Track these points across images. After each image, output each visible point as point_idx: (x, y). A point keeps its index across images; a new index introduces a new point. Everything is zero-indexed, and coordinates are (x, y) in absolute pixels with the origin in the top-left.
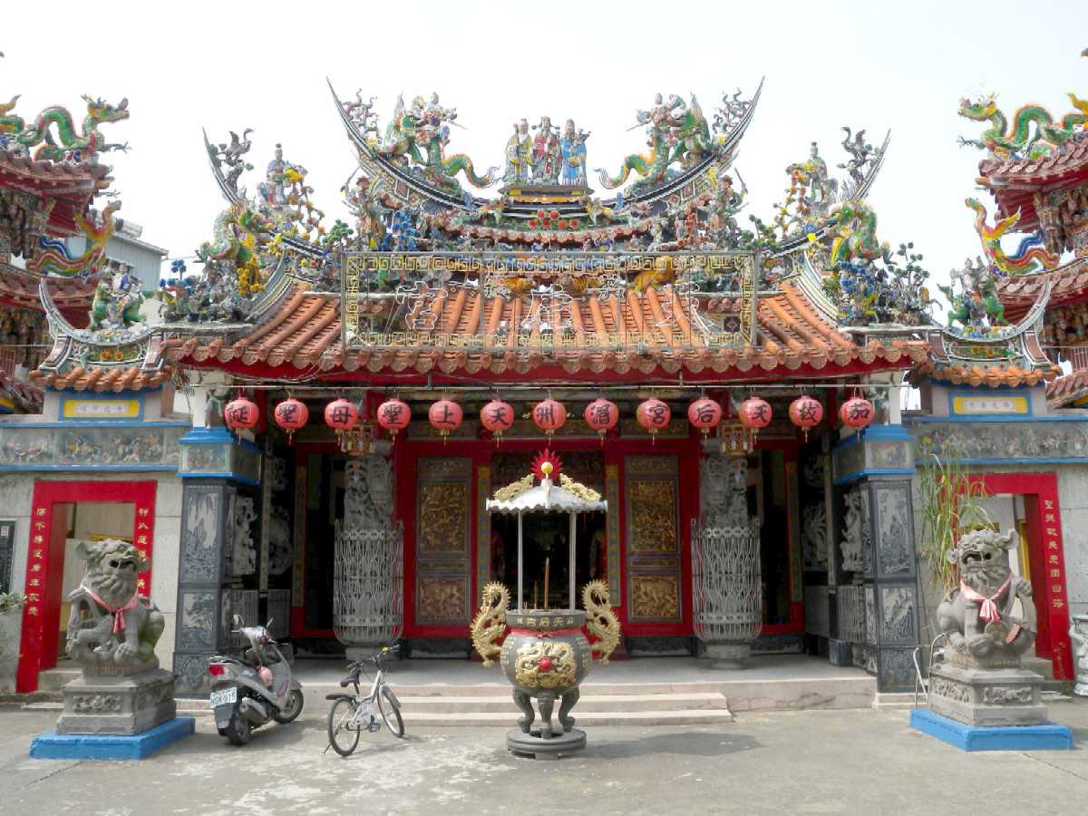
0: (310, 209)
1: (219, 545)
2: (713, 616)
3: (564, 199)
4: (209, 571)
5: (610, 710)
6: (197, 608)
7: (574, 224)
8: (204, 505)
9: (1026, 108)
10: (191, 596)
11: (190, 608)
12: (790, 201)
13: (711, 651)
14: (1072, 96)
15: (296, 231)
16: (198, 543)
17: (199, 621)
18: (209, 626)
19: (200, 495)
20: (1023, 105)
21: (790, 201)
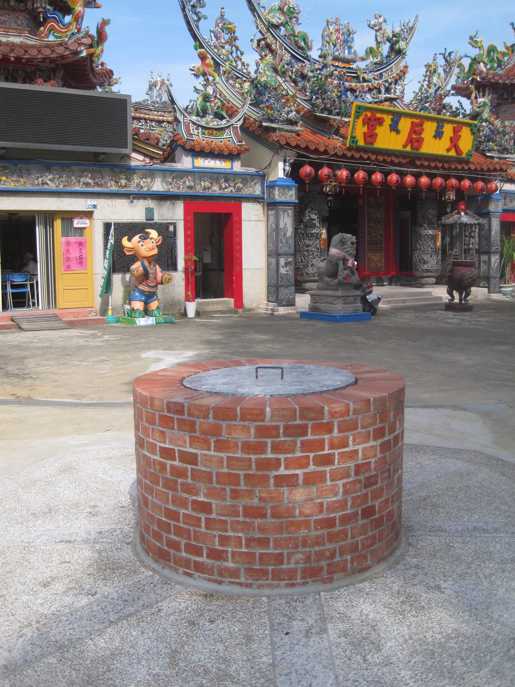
0: (237, 49)
1: (293, 235)
2: (426, 266)
3: (347, 66)
4: (290, 247)
5: (414, 299)
6: (287, 264)
7: (351, 79)
8: (286, 215)
9: (107, 39)
10: (283, 259)
11: (283, 265)
12: (424, 80)
13: (425, 280)
14: (505, 43)
15: (237, 66)
16: (285, 234)
17: (287, 271)
18: (291, 273)
19: (284, 211)
20: (108, 35)
21: (424, 80)
